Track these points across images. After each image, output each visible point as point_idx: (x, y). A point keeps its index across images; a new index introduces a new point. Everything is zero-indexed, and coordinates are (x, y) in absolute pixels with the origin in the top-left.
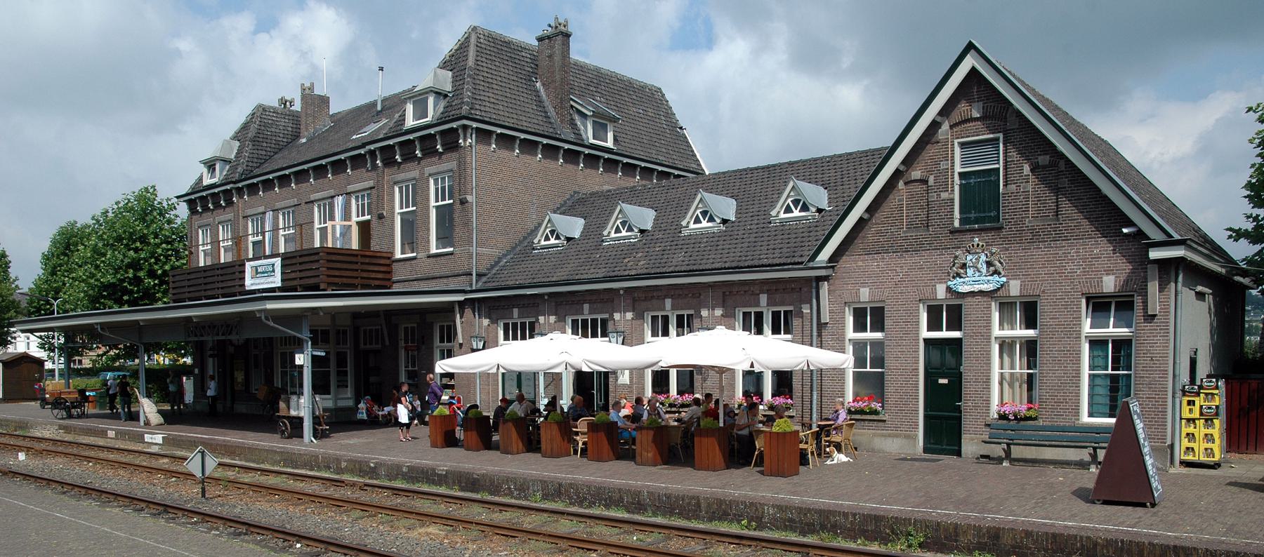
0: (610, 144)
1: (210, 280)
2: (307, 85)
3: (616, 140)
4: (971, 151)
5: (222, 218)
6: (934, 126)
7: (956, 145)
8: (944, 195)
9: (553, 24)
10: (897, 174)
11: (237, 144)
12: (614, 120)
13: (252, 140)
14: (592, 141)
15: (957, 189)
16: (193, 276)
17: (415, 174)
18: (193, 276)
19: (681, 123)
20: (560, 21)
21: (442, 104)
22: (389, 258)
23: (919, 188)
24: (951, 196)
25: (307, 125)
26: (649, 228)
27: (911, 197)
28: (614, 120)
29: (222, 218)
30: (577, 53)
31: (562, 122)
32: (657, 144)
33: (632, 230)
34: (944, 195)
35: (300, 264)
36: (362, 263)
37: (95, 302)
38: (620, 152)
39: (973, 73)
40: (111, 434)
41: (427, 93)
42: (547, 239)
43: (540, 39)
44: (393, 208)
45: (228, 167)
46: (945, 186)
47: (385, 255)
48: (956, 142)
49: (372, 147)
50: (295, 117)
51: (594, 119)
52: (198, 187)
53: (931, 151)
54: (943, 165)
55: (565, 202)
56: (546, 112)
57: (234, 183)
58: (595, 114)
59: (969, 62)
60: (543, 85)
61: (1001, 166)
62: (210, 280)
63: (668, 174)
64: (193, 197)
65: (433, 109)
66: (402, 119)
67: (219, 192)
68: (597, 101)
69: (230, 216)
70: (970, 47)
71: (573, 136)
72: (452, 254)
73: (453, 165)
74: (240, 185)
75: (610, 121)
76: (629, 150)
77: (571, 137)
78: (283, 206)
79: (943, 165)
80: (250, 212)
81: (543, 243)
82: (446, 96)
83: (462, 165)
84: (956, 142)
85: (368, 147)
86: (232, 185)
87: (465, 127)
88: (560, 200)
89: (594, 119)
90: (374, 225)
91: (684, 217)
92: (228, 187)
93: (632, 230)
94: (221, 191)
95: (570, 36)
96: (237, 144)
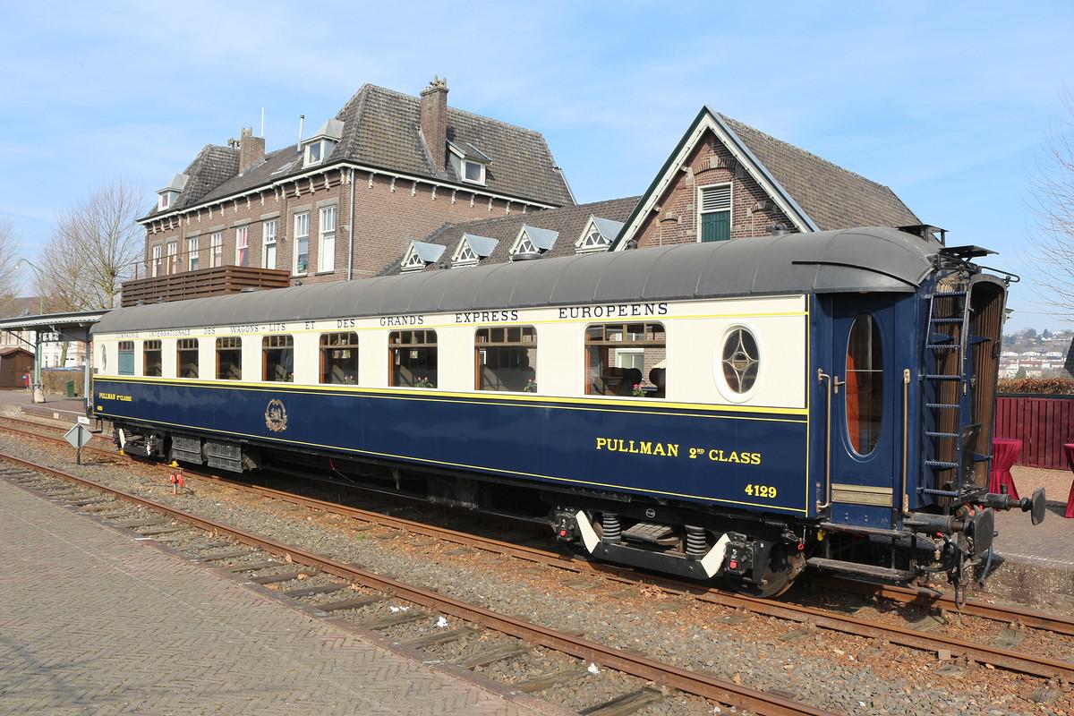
0: (482, 181)
1: (150, 290)
2: (247, 129)
3: (488, 175)
4: (710, 194)
5: (170, 239)
6: (681, 174)
7: (699, 190)
8: (689, 232)
9: (433, 82)
10: (653, 213)
11: (188, 177)
12: (485, 161)
13: (198, 175)
14: (464, 179)
15: (699, 227)
16: (149, 285)
17: (309, 206)
18: (149, 285)
19: (557, 164)
20: (439, 79)
21: (333, 147)
22: (287, 276)
23: (670, 225)
24: (694, 233)
25: (244, 162)
26: (550, 249)
27: (666, 233)
28: (485, 161)
29: (170, 239)
30: (453, 102)
31: (437, 163)
32: (530, 182)
33: (604, 242)
34: (689, 232)
35: (213, 279)
36: (263, 280)
37: (797, 230)
38: (490, 189)
39: (709, 133)
40: (56, 416)
41: (319, 139)
42: (412, 263)
43: (423, 95)
44: (293, 234)
45: (177, 197)
46: (690, 225)
47: (284, 273)
48: (699, 188)
49: (278, 183)
50: (236, 156)
51: (469, 161)
52: (154, 213)
53: (676, 196)
54: (689, 208)
55: (437, 231)
56: (424, 155)
57: (179, 210)
58: (467, 157)
59: (707, 122)
60: (424, 132)
61: (731, 209)
62: (150, 290)
63: (539, 208)
64: (149, 221)
65: (324, 150)
66: (301, 163)
67: (160, 220)
68: (475, 145)
69: (176, 238)
70: (705, 110)
71: (446, 175)
72: (306, 276)
73: (336, 200)
74: (184, 212)
75: (483, 163)
76: (500, 187)
77: (445, 176)
78: (215, 230)
79: (689, 208)
80: (190, 234)
81: (408, 266)
82: (336, 142)
83: (343, 200)
84: (699, 188)
85: (275, 184)
86: (177, 212)
87: (345, 169)
88: (433, 230)
89: (469, 161)
90: (251, 250)
91: (577, 239)
92: (175, 213)
93: (604, 242)
94: (262, 191)
95: (447, 92)
96: (188, 177)
